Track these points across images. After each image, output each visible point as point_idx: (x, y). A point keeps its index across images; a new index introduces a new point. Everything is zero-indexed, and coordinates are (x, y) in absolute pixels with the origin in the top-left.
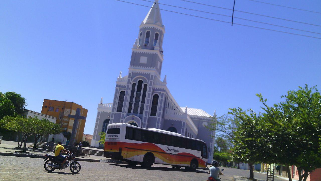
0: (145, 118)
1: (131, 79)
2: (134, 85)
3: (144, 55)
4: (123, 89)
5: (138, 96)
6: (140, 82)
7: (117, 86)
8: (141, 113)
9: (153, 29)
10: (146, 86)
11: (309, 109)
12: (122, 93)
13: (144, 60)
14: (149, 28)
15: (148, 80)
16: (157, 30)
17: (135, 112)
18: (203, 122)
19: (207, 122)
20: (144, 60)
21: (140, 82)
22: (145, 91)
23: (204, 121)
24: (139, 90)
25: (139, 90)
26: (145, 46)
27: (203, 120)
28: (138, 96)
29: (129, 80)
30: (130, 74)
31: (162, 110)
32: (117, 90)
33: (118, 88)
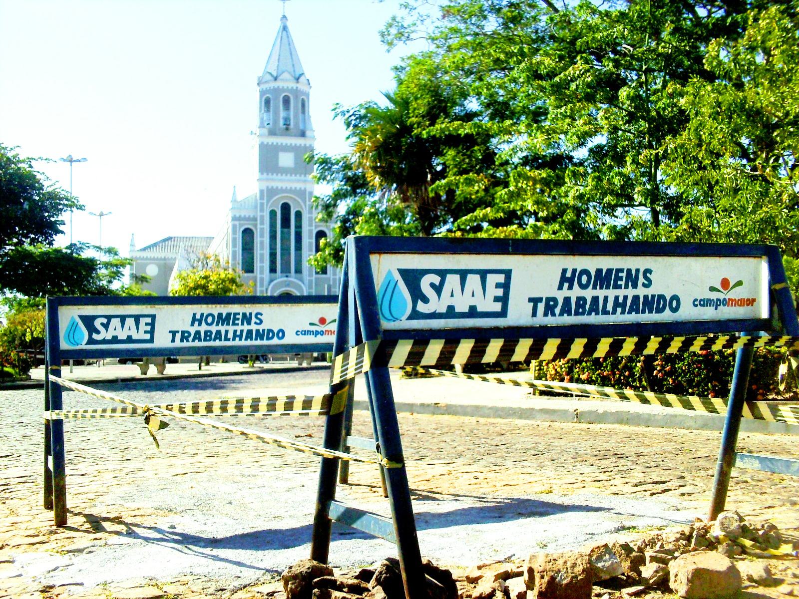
0: (310, 281)
1: (265, 201)
2: (273, 213)
3: (286, 149)
4: (249, 224)
5: (285, 239)
6: (286, 208)
7: (234, 219)
8: (298, 271)
9: (276, 91)
10: (299, 215)
11: (754, 212)
12: (248, 234)
13: (286, 160)
14: (288, 90)
15: (302, 200)
16: (283, 90)
17: (286, 270)
18: (147, 265)
19: (155, 263)
20: (286, 160)
21: (286, 208)
22: (299, 226)
23: (150, 263)
24: (286, 222)
25: (286, 222)
26: (287, 129)
27: (145, 262)
28: (285, 239)
29: (262, 205)
30: (262, 192)
31: (259, 256)
32: (234, 227)
33: (237, 223)
